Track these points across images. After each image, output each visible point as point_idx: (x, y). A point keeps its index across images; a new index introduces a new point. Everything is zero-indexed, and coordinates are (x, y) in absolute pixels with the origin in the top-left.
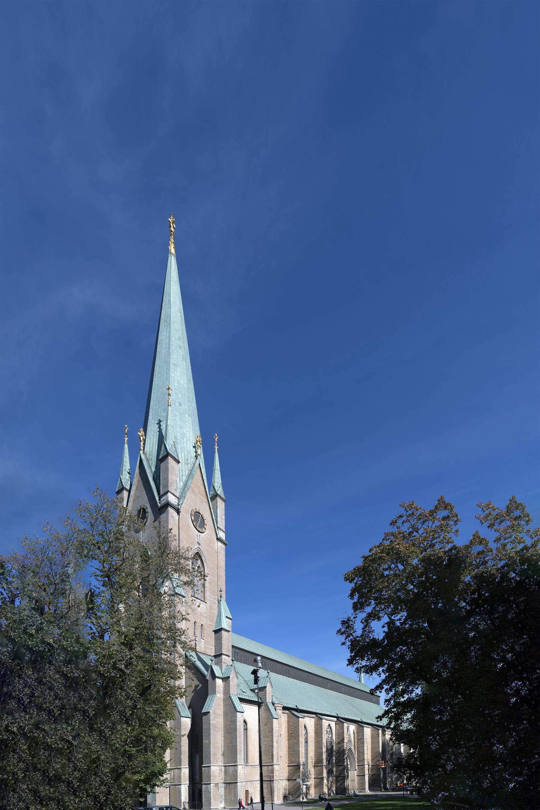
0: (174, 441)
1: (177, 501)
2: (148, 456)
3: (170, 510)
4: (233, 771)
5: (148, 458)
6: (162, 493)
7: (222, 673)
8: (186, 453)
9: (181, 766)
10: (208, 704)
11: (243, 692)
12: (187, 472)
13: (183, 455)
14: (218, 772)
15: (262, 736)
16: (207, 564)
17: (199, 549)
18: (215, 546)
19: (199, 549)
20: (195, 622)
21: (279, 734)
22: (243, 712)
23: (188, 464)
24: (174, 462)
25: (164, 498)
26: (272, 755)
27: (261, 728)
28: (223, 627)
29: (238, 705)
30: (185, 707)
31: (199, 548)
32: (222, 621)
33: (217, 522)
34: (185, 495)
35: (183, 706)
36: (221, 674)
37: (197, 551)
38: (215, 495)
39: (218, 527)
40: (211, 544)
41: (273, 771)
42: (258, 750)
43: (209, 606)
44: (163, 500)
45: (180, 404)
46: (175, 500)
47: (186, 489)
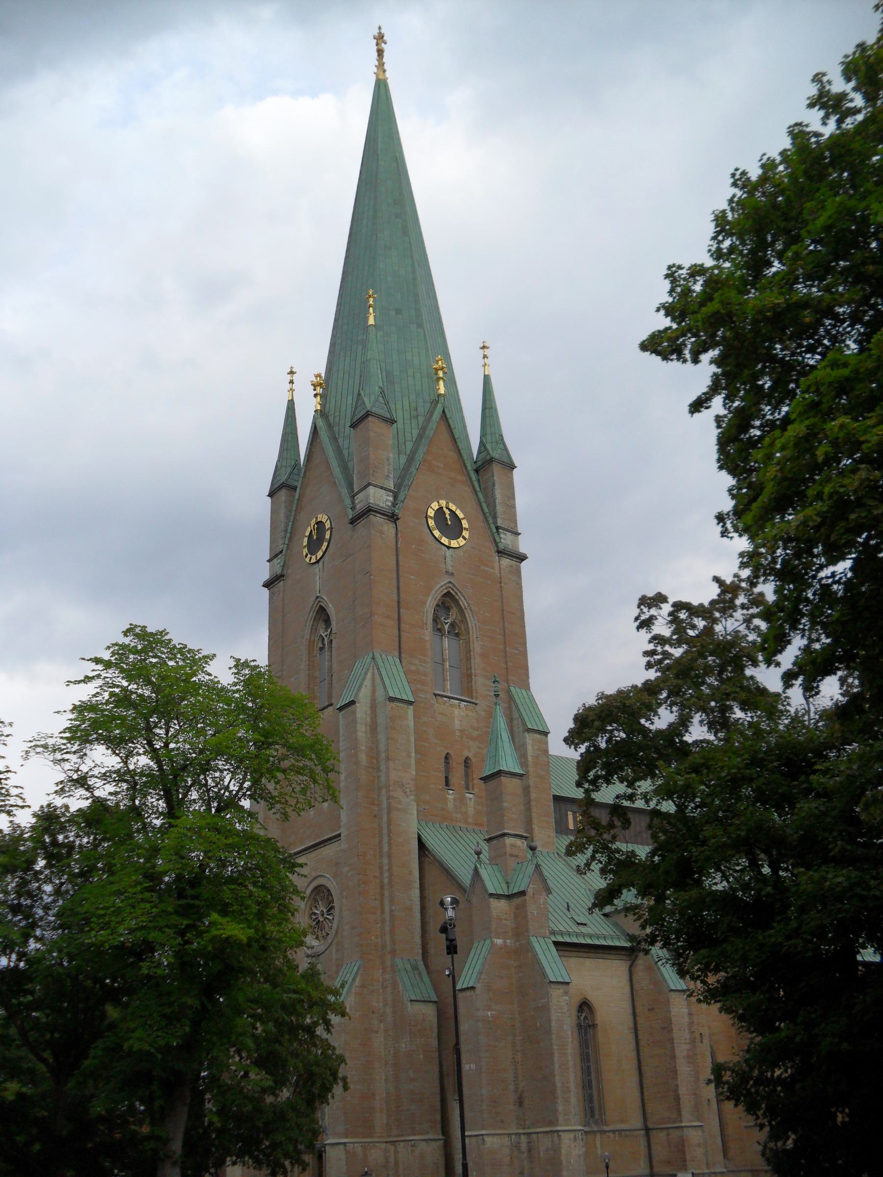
0: (381, 385)
1: (391, 499)
2: (331, 419)
3: (378, 519)
4: (547, 1150)
5: (332, 422)
6: (356, 488)
7: (507, 883)
8: (413, 397)
9: (681, 1122)
10: (473, 966)
11: (578, 924)
12: (415, 432)
13: (406, 403)
14: (506, 1151)
15: (642, 1043)
16: (472, 614)
17: (451, 585)
18: (493, 568)
19: (451, 585)
20: (448, 754)
21: (697, 1035)
22: (568, 983)
23: (417, 417)
24: (383, 425)
25: (360, 497)
26: (677, 1098)
27: (640, 1021)
28: (504, 768)
29: (554, 966)
30: (420, 974)
31: (450, 582)
32: (501, 753)
33: (495, 517)
34: (409, 481)
35: (416, 972)
36: (504, 886)
37: (446, 591)
38: (487, 461)
39: (497, 528)
40: (482, 568)
41: (683, 1146)
42: (465, 1106)
43: (484, 711)
44: (359, 502)
45: (398, 311)
46: (385, 497)
47: (413, 469)
